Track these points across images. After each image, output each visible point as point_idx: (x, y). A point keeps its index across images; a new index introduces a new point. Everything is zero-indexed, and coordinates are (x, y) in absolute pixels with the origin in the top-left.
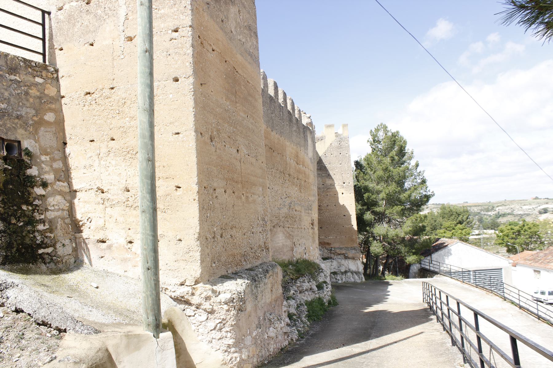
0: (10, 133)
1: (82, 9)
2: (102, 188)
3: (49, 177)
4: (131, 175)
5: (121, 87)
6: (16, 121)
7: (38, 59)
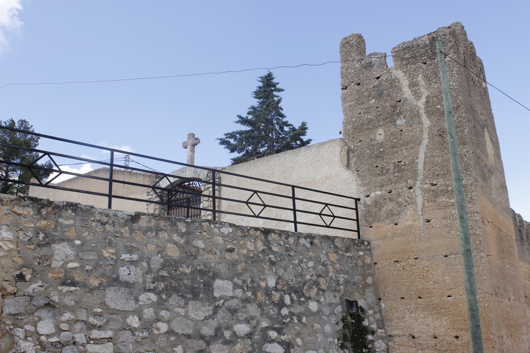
0: (351, 296)
1: (385, 197)
2: (414, 335)
3: (374, 326)
4: (437, 326)
5: (424, 258)
6: (354, 287)
7: (355, 236)
